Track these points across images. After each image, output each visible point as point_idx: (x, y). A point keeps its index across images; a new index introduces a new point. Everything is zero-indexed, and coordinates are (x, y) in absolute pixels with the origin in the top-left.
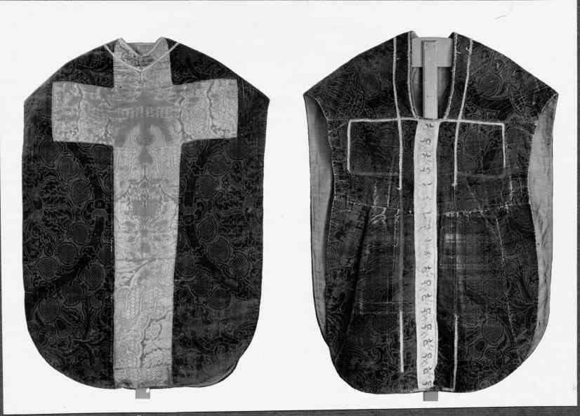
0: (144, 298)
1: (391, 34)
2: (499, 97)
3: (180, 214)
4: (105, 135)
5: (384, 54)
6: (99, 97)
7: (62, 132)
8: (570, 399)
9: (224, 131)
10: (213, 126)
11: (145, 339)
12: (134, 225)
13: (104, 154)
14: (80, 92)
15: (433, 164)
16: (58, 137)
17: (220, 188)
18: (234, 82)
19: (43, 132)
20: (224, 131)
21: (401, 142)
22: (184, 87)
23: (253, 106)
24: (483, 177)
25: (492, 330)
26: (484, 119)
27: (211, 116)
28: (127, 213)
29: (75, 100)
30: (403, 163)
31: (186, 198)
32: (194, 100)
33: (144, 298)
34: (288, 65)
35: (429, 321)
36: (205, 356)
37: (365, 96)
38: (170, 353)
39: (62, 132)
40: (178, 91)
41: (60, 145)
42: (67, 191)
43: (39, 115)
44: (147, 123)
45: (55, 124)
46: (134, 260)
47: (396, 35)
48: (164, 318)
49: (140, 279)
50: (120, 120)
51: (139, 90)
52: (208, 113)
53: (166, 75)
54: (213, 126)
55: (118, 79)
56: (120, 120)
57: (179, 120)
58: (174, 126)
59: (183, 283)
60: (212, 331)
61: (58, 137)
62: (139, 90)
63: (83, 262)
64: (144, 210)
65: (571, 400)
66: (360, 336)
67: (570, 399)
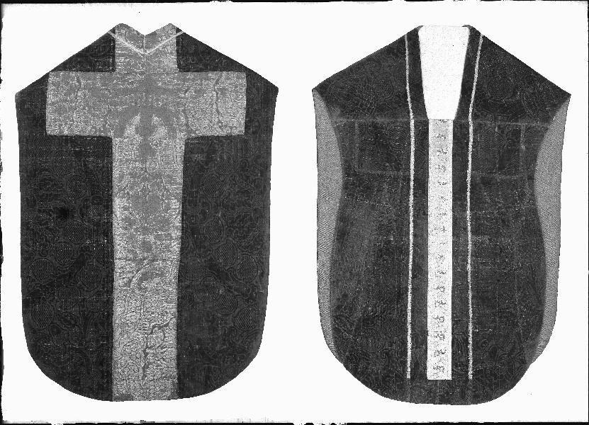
0: (144, 312)
1: (402, 31)
2: (510, 97)
3: (183, 214)
4: (104, 126)
5: (397, 56)
6: (99, 85)
7: (55, 125)
8: (586, 420)
9: (231, 128)
10: (219, 122)
11: (147, 347)
12: (134, 222)
13: (103, 146)
14: (79, 81)
15: (432, 264)
16: (52, 129)
17: (227, 185)
18: (244, 75)
19: (36, 126)
20: (231, 128)
21: (413, 140)
22: (190, 75)
23: (262, 96)
24: (499, 177)
25: (505, 332)
26: (472, 304)
27: (217, 110)
28: (125, 208)
29: (73, 90)
30: (415, 161)
31: (188, 201)
32: (200, 92)
33: (144, 312)
34: (299, 55)
35: (441, 348)
36: (213, 366)
37: (372, 97)
38: (174, 363)
39: (55, 125)
40: (184, 80)
41: (59, 139)
42: (66, 184)
43: (31, 103)
44: (148, 111)
45: (50, 116)
46: (134, 260)
47: (406, 33)
48: (167, 325)
49: (141, 280)
50: (120, 109)
51: (142, 74)
52: (215, 106)
53: (171, 61)
54: (219, 122)
55: (120, 61)
56: (120, 109)
57: (184, 111)
58: (178, 118)
59: (188, 287)
60: (217, 342)
61: (52, 129)
62: (142, 74)
63: (80, 263)
64: (146, 204)
65: (587, 420)
66: (371, 338)
67: (586, 420)
